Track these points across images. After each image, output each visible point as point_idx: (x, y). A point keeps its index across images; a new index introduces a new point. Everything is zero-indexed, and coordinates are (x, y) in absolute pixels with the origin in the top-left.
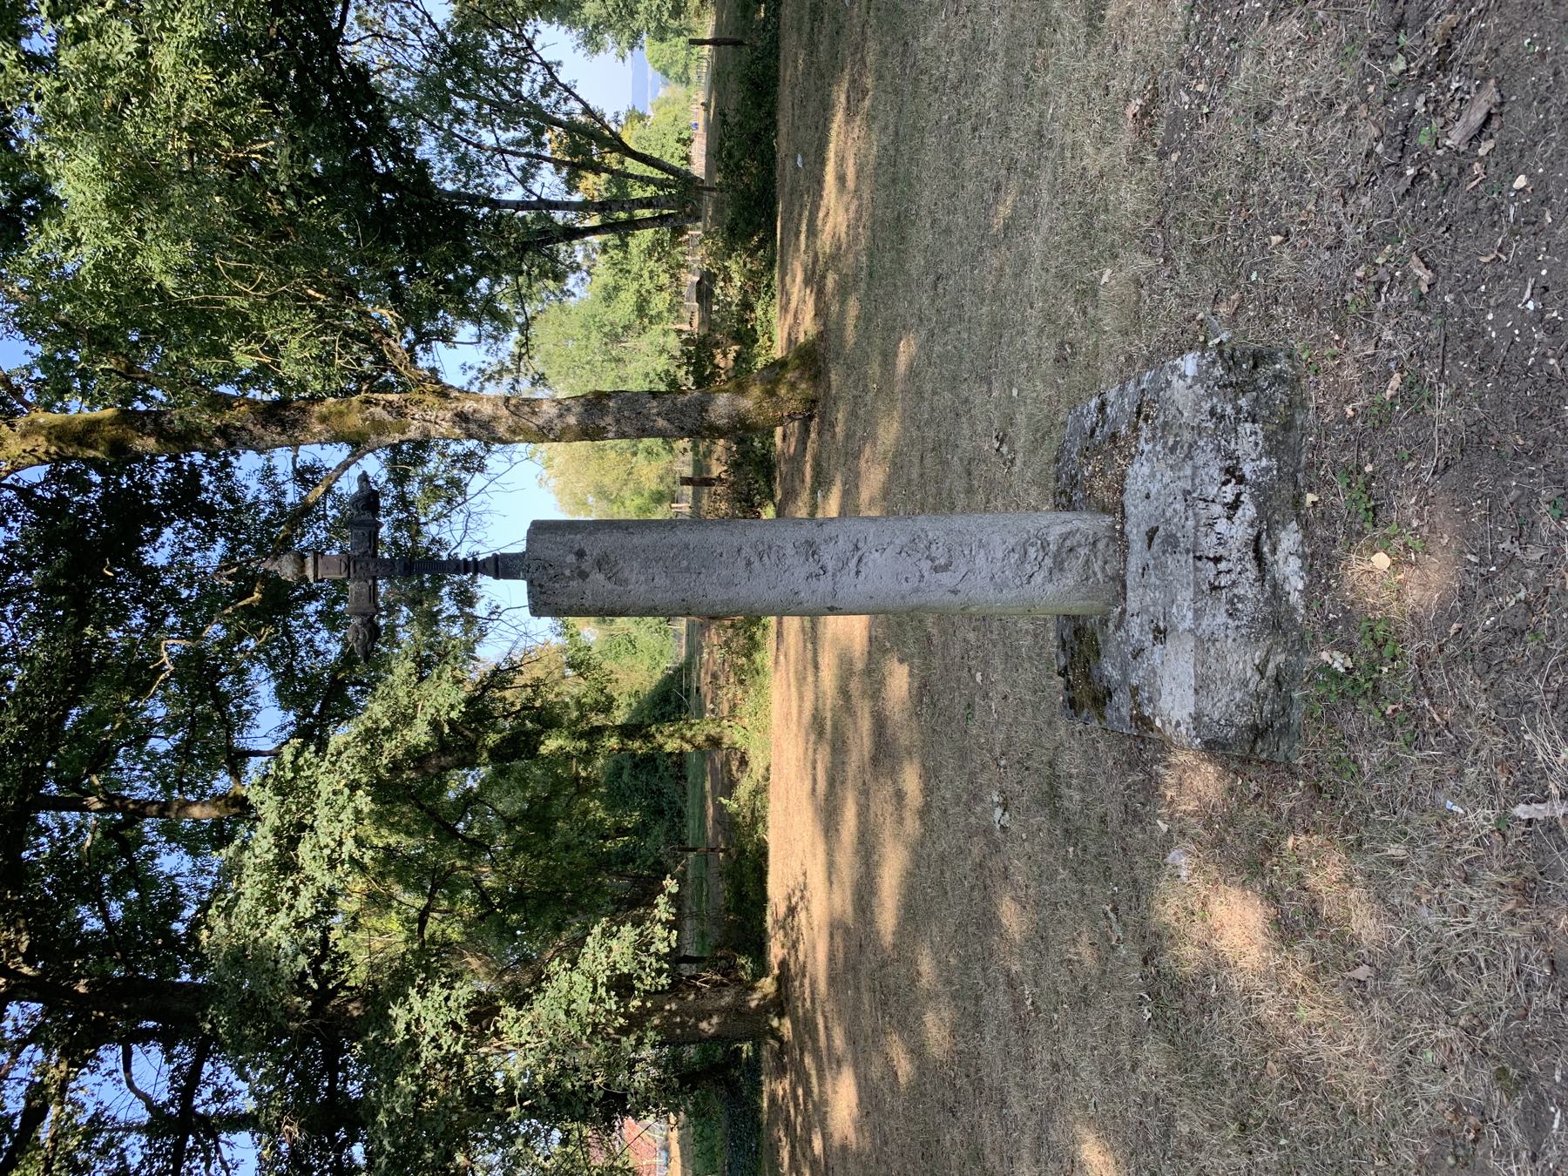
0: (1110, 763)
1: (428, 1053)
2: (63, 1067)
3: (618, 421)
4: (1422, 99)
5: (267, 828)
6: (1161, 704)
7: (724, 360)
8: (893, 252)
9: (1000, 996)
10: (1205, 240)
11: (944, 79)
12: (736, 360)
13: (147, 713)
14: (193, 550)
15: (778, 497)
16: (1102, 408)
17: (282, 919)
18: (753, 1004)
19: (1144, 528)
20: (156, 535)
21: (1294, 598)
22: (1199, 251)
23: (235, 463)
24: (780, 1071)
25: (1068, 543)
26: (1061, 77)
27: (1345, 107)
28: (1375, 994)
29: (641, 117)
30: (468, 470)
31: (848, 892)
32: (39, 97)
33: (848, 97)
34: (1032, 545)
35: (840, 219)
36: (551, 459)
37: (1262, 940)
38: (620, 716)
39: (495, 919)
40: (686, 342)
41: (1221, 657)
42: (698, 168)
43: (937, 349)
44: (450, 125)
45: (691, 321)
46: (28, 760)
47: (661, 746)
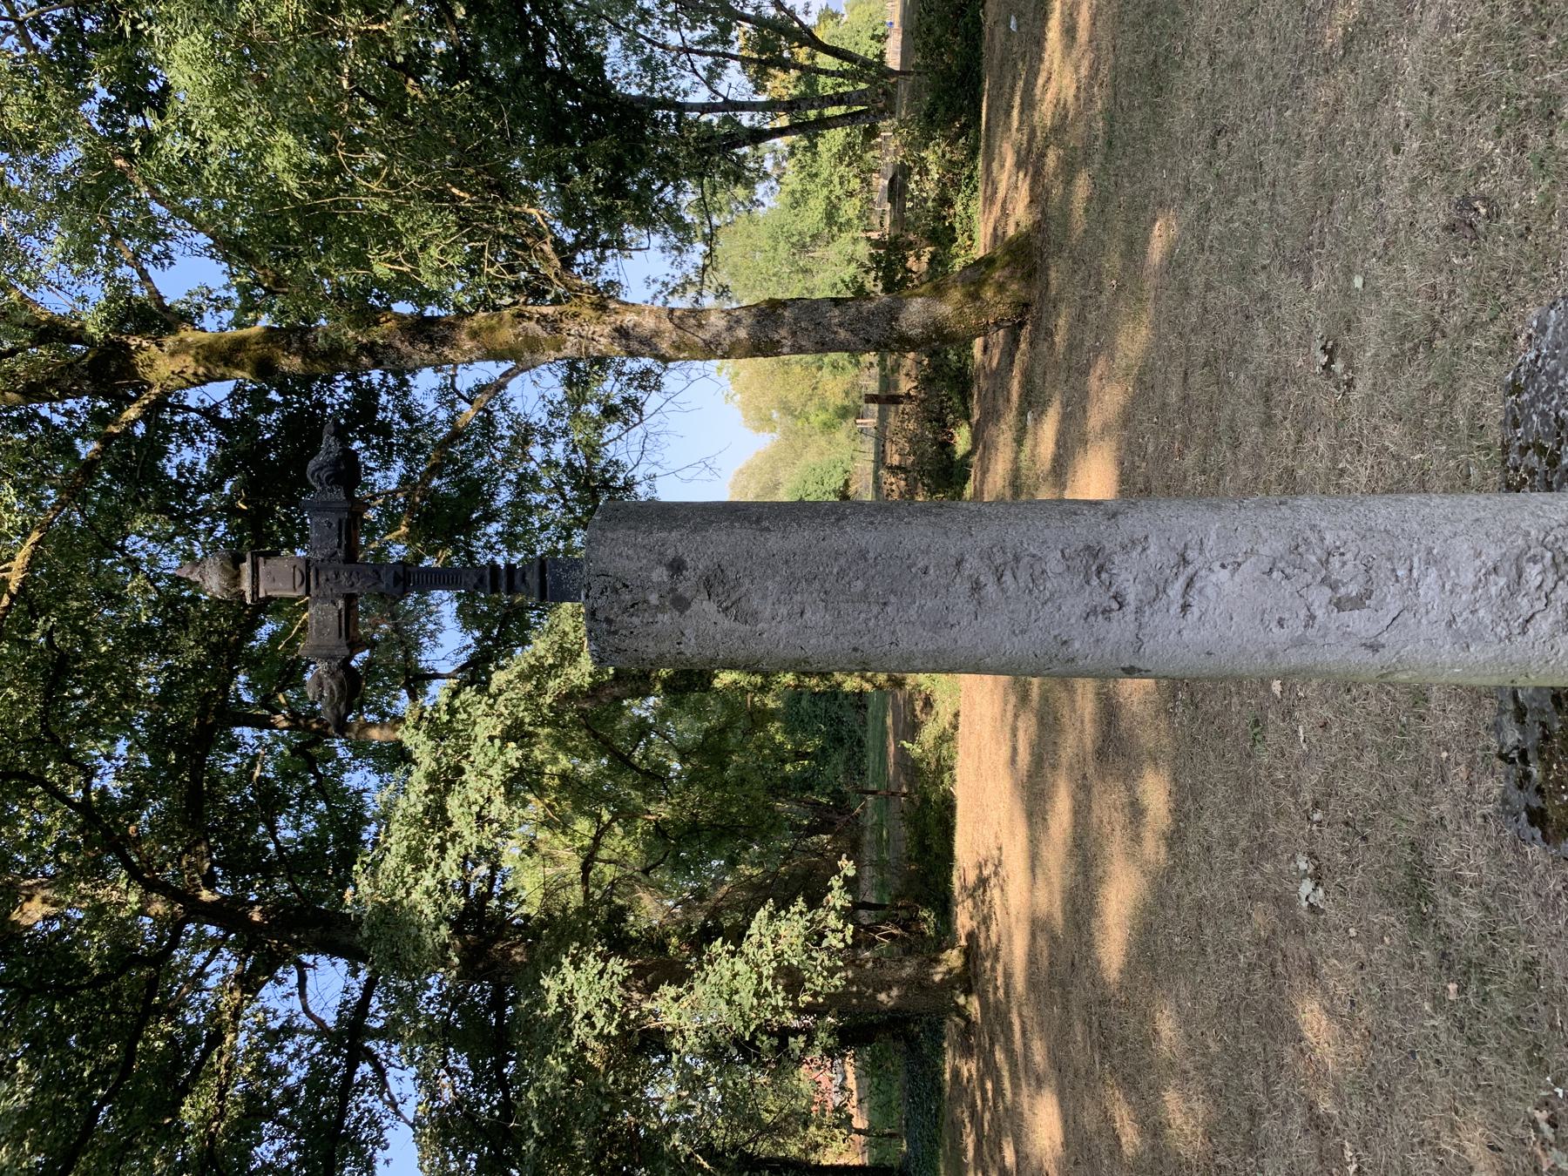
1: (580, 1031)
2: (237, 994)
3: (794, 334)
5: (421, 773)
7: (918, 264)
12: (930, 262)
15: (976, 417)
18: (937, 978)
24: (966, 1051)
29: (834, 15)
30: (644, 388)
34: (1534, 560)
35: (1066, 82)
36: (737, 374)
42: (894, 61)
43: (1215, 228)
45: (883, 226)
47: (839, 685)
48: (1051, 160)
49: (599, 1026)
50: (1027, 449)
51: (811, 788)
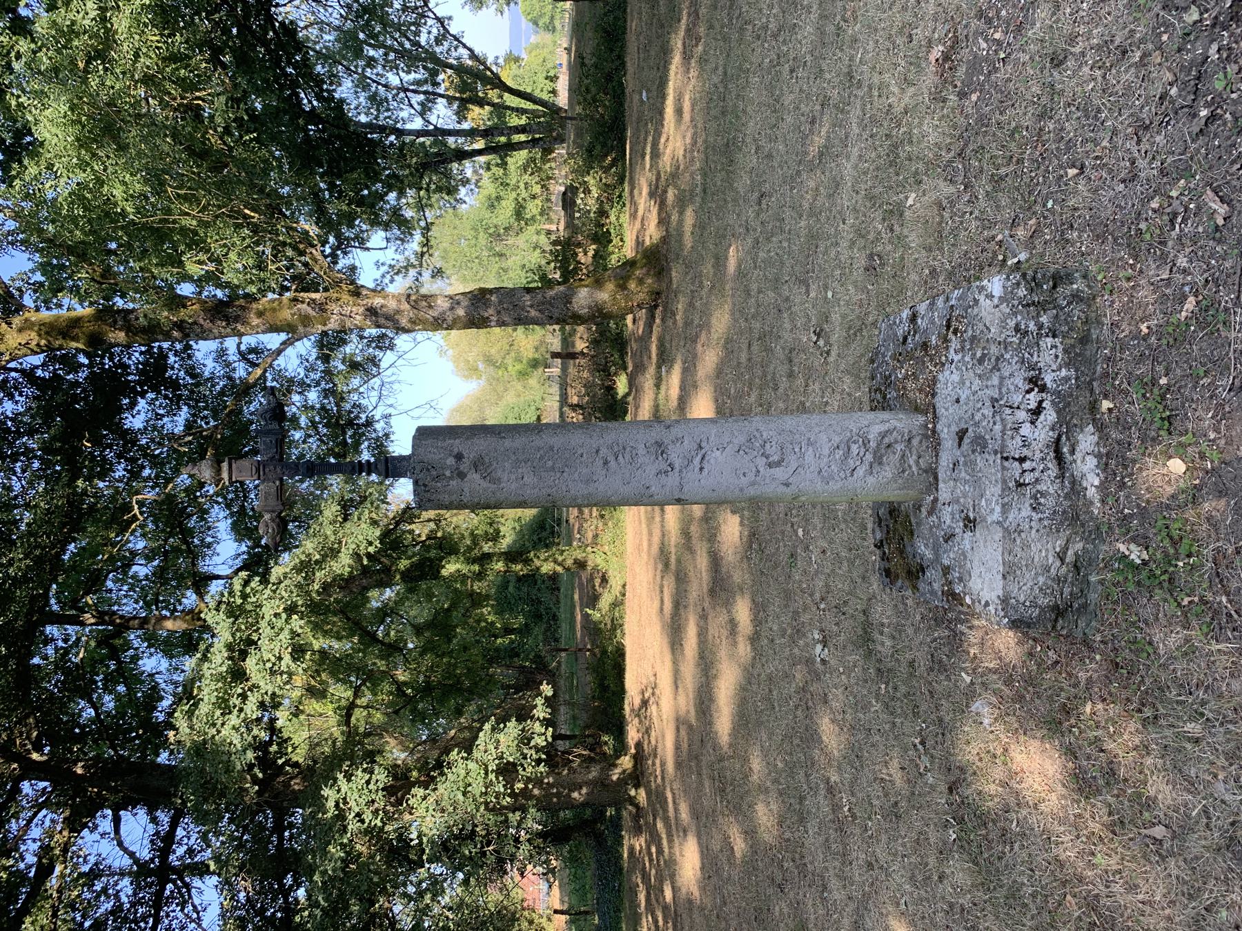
0: (918, 617)
1: (353, 826)
3: (499, 312)
4: (1215, 47)
6: (971, 584)
7: (585, 257)
8: (723, 173)
9: (821, 798)
10: (1003, 171)
11: (766, 28)
12: (594, 257)
13: (130, 545)
14: (163, 416)
15: (630, 369)
16: (913, 318)
17: (234, 720)
18: (615, 778)
19: (954, 428)
20: (133, 404)
21: (1092, 492)
22: (997, 181)
23: (195, 346)
24: (637, 831)
25: (886, 440)
26: (869, 27)
27: (1138, 54)
28: (1171, 854)
29: (517, 60)
31: (691, 696)
32: (18, 56)
33: (684, 44)
34: (855, 442)
37: (1060, 789)
38: (506, 543)
39: (409, 706)
40: (554, 243)
41: (1026, 546)
42: (562, 100)
44: (363, 70)
45: (558, 224)
46: (32, 589)
47: (538, 569)
48: (671, 194)
49: (367, 821)
50: (663, 391)
51: (518, 655)
